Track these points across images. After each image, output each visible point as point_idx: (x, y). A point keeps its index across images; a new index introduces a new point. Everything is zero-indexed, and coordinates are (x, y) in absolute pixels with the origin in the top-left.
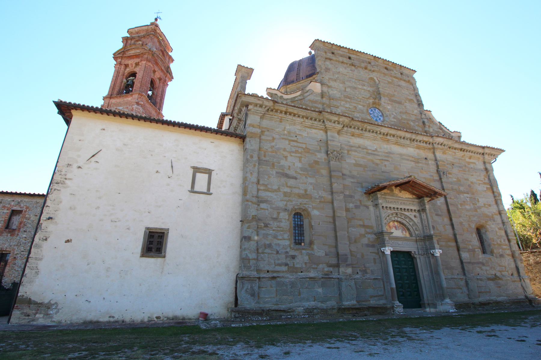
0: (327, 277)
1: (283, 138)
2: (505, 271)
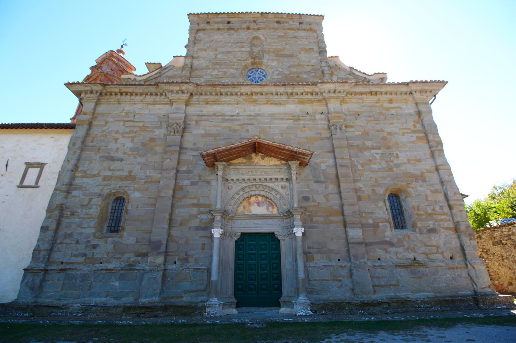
0: (130, 268)
1: (117, 121)
2: (437, 252)
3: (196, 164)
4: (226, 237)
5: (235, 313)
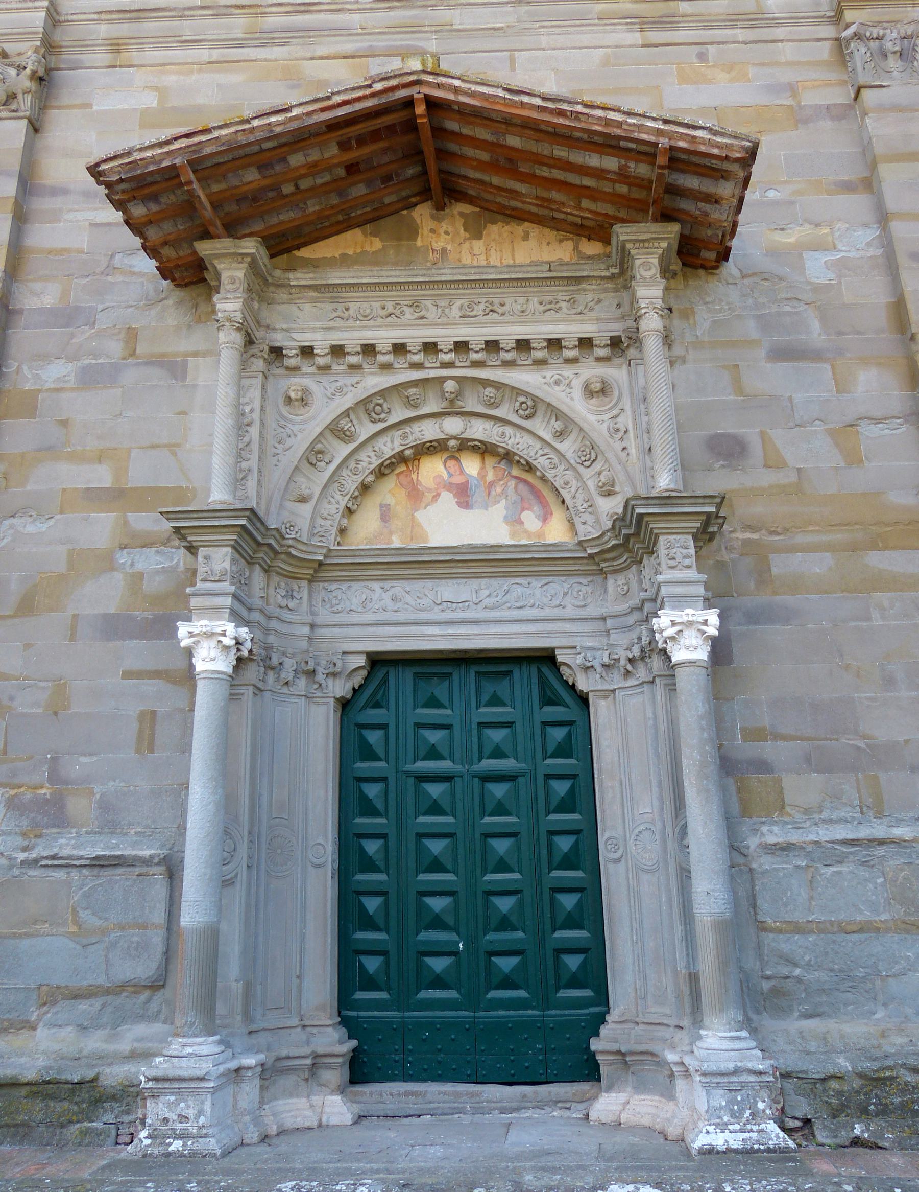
3: (111, 269)
4: (278, 680)
5: (334, 1121)
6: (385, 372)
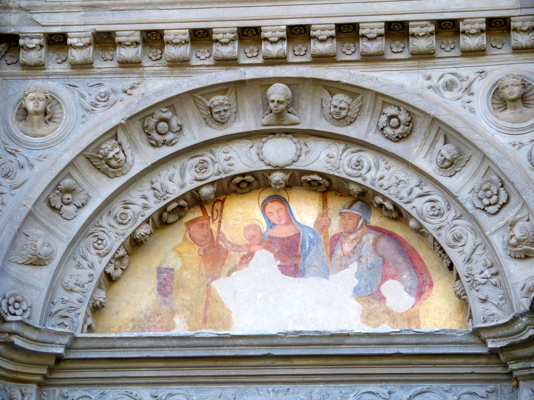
6: (177, 71)
